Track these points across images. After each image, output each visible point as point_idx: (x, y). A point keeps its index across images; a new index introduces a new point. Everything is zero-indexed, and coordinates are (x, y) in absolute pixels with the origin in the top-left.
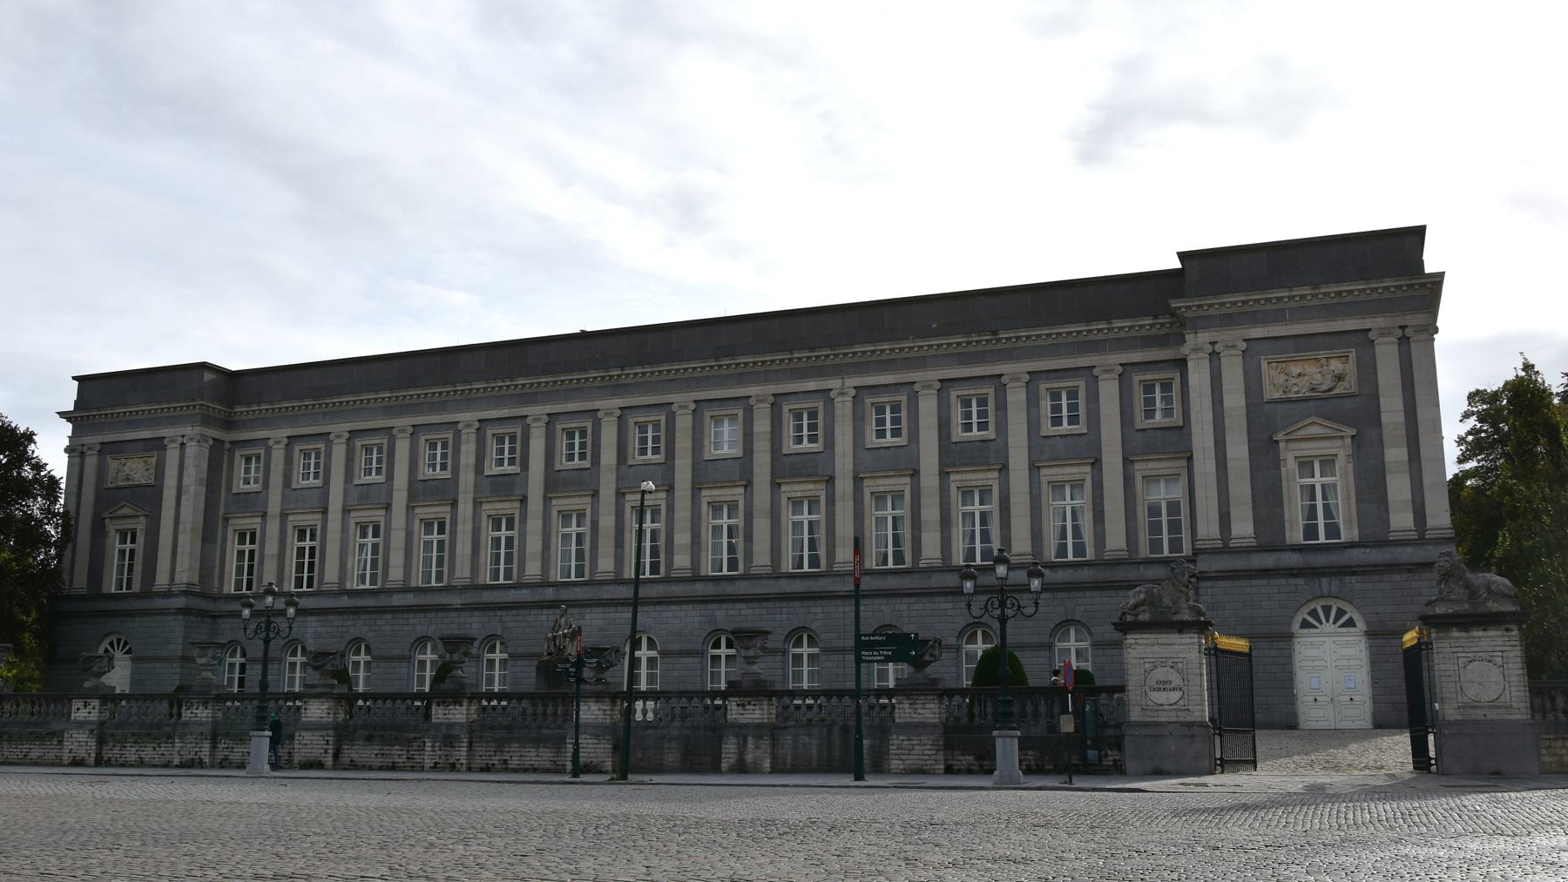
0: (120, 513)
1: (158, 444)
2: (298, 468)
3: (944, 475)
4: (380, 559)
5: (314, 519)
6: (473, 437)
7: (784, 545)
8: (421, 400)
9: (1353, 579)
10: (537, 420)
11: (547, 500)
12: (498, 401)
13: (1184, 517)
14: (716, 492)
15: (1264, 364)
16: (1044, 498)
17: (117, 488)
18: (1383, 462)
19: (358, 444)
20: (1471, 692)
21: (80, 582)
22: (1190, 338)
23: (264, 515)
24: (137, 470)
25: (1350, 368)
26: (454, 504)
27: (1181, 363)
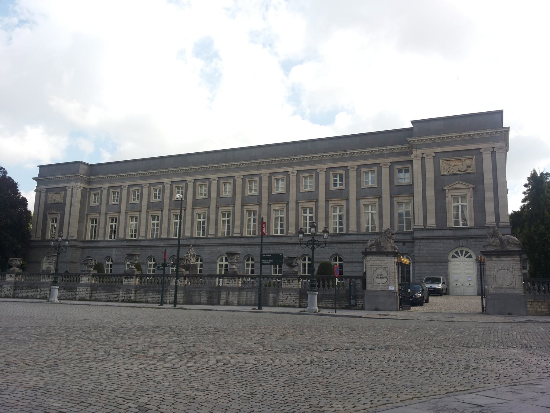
0: (51, 212)
1: (64, 189)
2: (153, 195)
3: (327, 201)
4: (230, 225)
5: (115, 215)
6: (169, 187)
7: (271, 226)
8: (152, 175)
9: (472, 240)
10: (190, 182)
11: (193, 209)
12: (177, 174)
13: (411, 217)
14: (249, 207)
15: (441, 162)
16: (361, 210)
17: (51, 204)
18: (484, 198)
19: (131, 189)
20: (500, 282)
21: (39, 236)
22: (414, 152)
23: (100, 214)
24: (57, 198)
25: (474, 162)
26: (162, 210)
27: (411, 162)
